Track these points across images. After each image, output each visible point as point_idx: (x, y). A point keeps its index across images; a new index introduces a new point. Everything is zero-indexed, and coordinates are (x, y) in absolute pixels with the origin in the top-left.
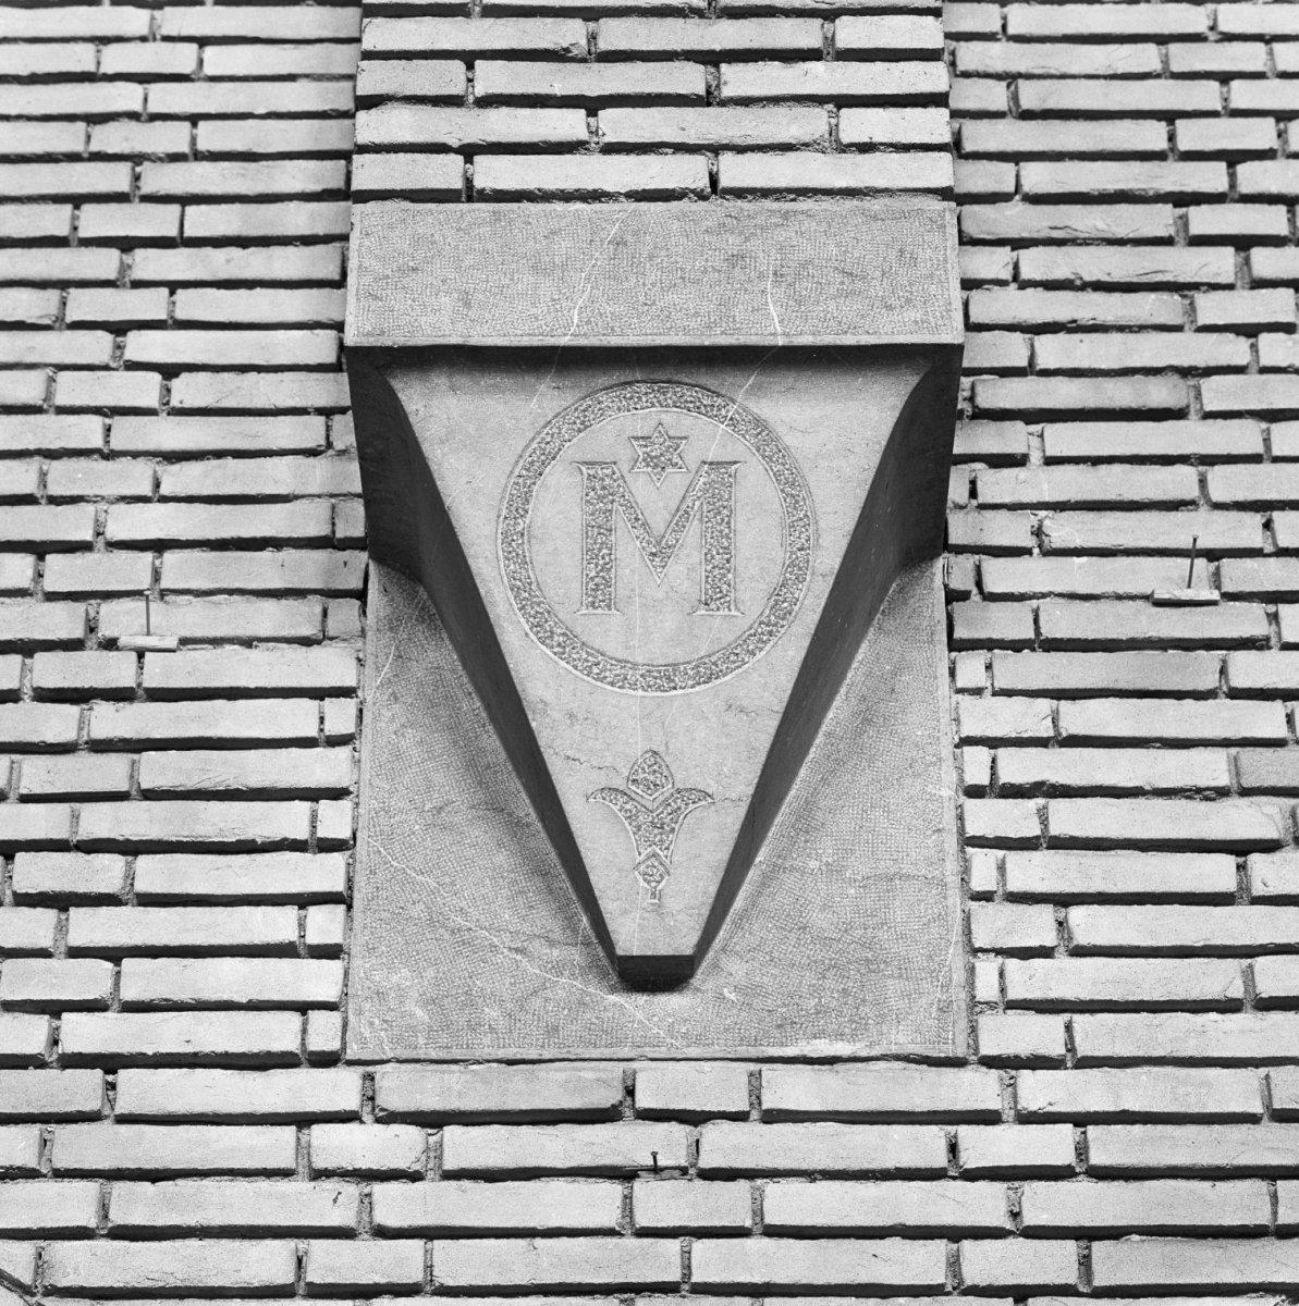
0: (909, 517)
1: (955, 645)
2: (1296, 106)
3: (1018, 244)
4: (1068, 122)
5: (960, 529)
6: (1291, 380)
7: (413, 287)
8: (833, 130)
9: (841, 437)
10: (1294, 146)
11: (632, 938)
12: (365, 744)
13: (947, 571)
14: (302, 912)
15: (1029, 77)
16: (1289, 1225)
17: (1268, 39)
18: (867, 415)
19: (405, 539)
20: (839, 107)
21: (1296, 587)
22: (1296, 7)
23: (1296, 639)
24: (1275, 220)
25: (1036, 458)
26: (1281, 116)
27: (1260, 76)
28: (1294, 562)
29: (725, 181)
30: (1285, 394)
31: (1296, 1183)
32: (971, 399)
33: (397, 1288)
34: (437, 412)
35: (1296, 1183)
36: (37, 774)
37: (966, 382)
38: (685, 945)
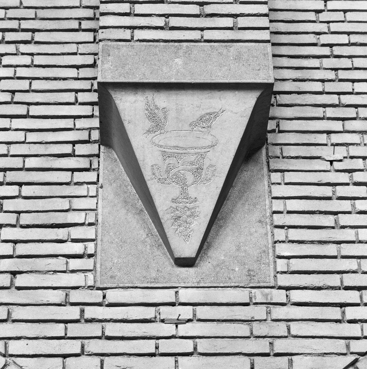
0: (254, 143)
1: (270, 171)
4: (303, 82)
6: (365, 25)
9: (238, 110)
10: (365, 301)
11: (177, 255)
16: (365, 286)
17: (356, 106)
18: (247, 102)
21: (366, 318)
22: (366, 2)
23: (366, 270)
24: (356, 330)
25: (326, 10)
27: (349, 213)
28: (366, 84)
30: (363, 100)
31: (366, 215)
33: (73, 256)
35: (366, 215)
36: (10, 37)
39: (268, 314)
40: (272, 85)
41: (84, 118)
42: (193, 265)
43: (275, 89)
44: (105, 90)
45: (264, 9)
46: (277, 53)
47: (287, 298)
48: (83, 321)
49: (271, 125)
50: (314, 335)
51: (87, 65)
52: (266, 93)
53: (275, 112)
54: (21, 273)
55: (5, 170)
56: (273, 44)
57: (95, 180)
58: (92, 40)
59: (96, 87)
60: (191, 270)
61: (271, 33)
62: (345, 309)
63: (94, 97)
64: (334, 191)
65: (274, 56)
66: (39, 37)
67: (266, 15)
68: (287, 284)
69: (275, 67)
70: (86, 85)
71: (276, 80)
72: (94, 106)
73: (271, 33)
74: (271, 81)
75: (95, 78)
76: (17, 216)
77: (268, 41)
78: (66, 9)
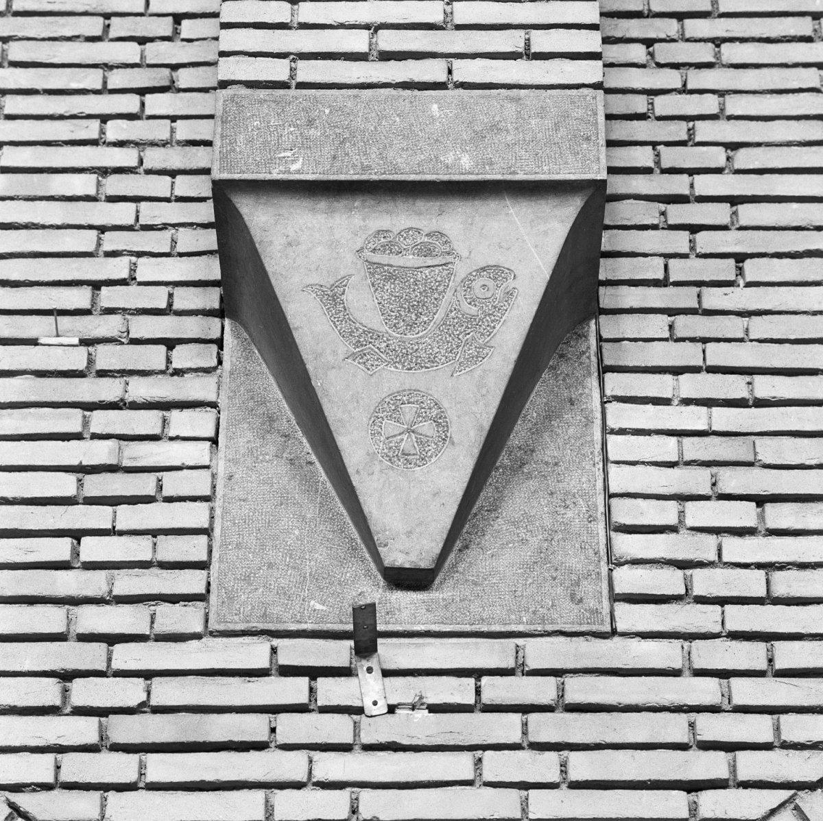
9: (532, 243)
18: (551, 226)
40: (603, 183)
41: (204, 146)
42: (426, 587)
45: (589, 13)
46: (615, 136)
47: (648, 17)
50: (694, 630)
51: (181, 197)
52: (595, 197)
54: (151, 40)
56: (609, 91)
64: (722, 102)
65: (611, 144)
67: (594, 27)
68: (648, 86)
69: (609, 117)
71: (612, 170)
72: (210, 203)
73: (605, 66)
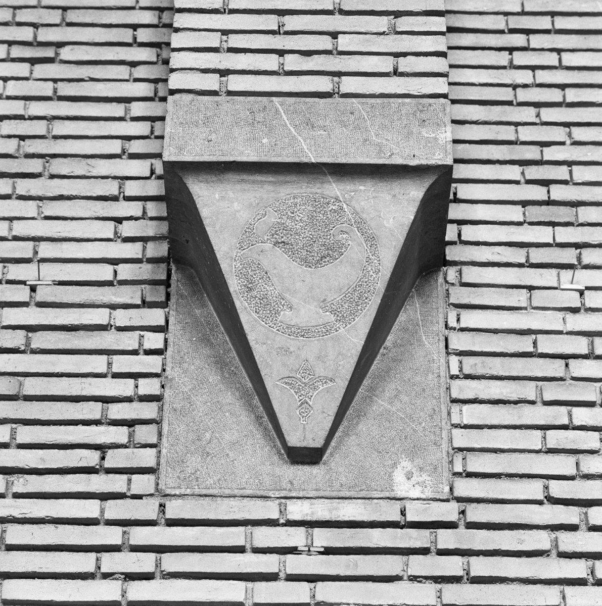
2: (601, 285)
3: (113, 307)
5: (452, 253)
7: (185, 143)
8: (511, 61)
9: (394, 211)
11: (294, 440)
12: (169, 352)
13: (445, 274)
14: (132, 429)
15: (344, 33)
18: (413, 193)
19: (185, 260)
20: (33, 65)
26: (457, 200)
29: (565, 63)
32: (455, 194)
34: (207, 196)
37: (454, 185)
38: (318, 443)
39: (434, 541)
40: (449, 169)
43: (455, 176)
44: (176, 175)
48: (157, 99)
49: (451, 233)
53: (455, 212)
55: (5, 79)
56: (454, 102)
57: (162, 322)
58: (148, 174)
59: (159, 170)
60: (314, 470)
61: (450, 84)
62: (580, 252)
63: (154, 188)
65: (456, 142)
66: (58, 167)
70: (140, 168)
71: (456, 161)
74: (449, 162)
75: (159, 156)
76: (34, 31)
77: (445, 96)
78: (104, 41)
